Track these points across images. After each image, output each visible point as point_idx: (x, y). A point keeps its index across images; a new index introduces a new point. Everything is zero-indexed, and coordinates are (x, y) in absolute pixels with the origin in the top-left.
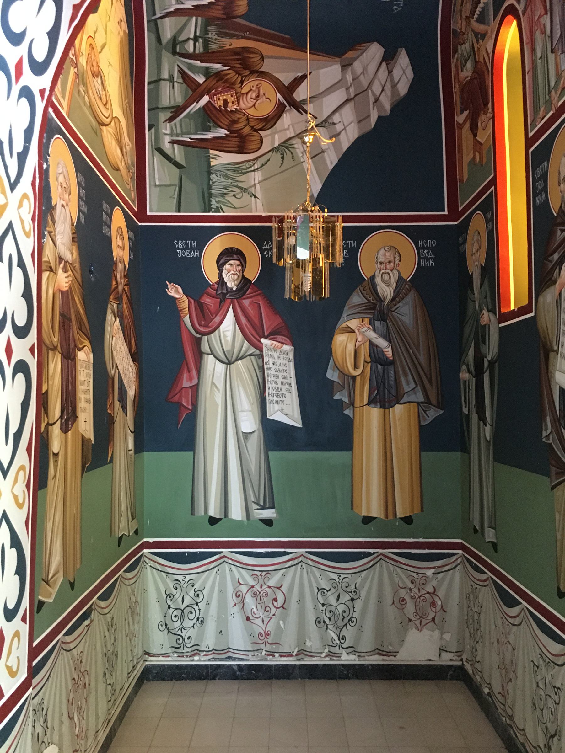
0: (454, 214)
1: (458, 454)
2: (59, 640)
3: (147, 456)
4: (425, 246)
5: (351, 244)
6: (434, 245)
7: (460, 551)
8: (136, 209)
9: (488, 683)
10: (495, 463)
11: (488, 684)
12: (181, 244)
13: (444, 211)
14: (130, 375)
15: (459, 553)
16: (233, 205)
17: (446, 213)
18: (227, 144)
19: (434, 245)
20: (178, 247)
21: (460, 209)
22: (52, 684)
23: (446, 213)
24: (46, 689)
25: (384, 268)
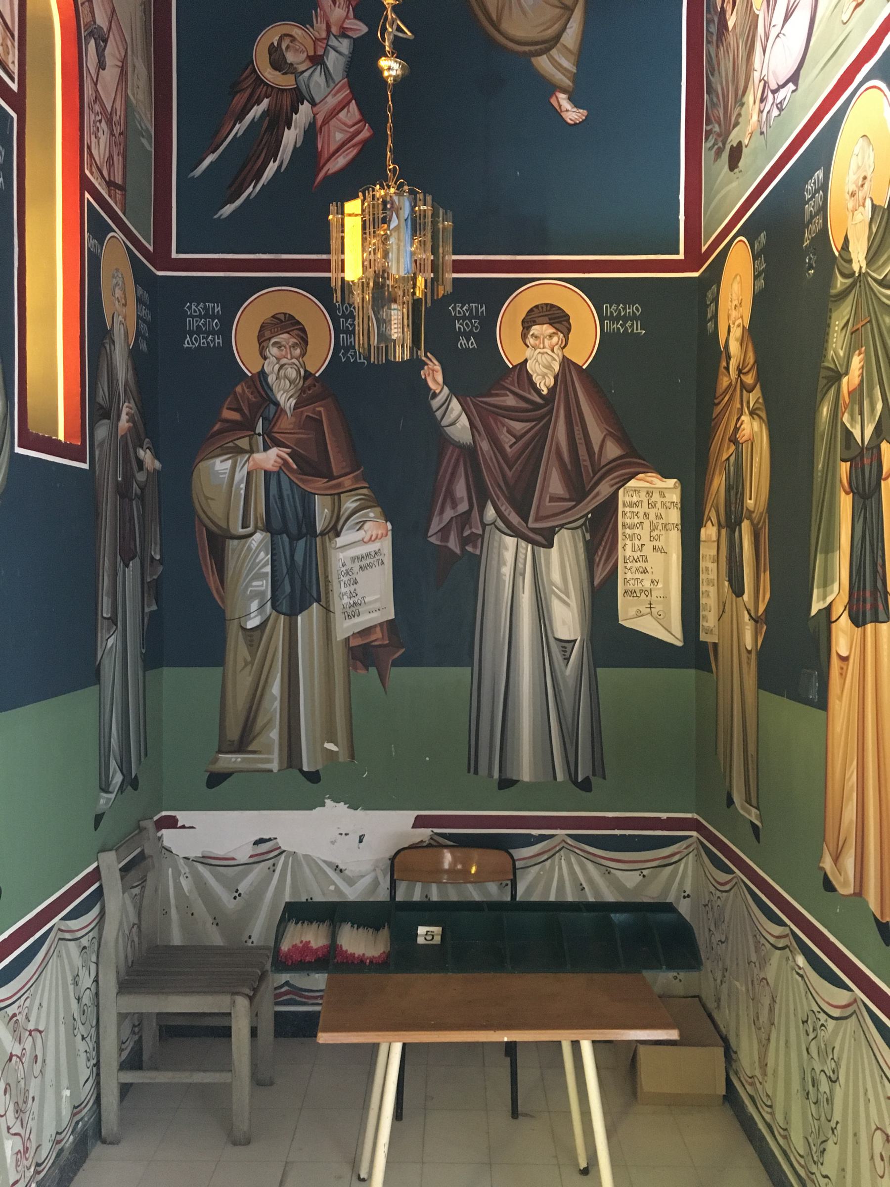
0: (694, 258)
1: (692, 672)
2: (53, 927)
3: (169, 674)
4: (622, 314)
5: (213, 308)
6: (638, 314)
7: (694, 834)
8: (151, 248)
9: (750, 1076)
10: (761, 691)
11: (750, 1078)
12: (195, 308)
13: (678, 253)
14: (384, 323)
15: (691, 836)
16: (97, 81)
17: (681, 256)
18: (287, 109)
19: (638, 314)
20: (191, 313)
21: (704, 249)
22: (52, 970)
23: (681, 256)
24: (46, 973)
25: (541, 346)
